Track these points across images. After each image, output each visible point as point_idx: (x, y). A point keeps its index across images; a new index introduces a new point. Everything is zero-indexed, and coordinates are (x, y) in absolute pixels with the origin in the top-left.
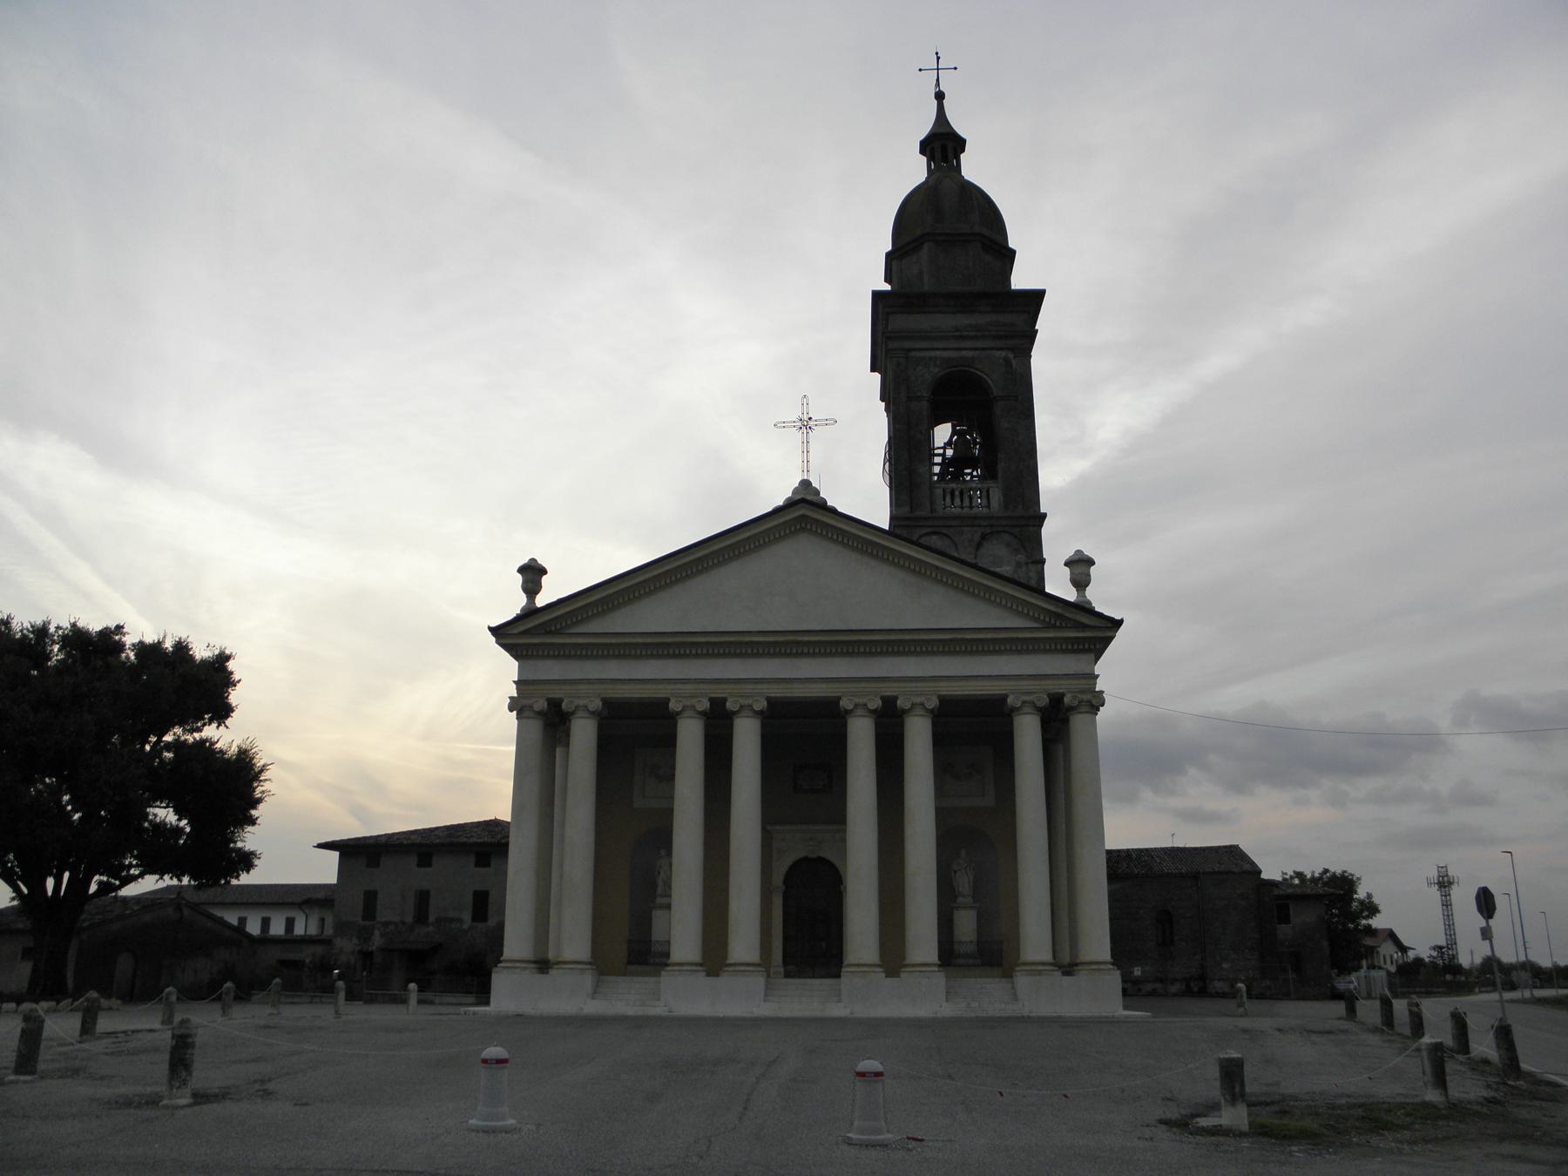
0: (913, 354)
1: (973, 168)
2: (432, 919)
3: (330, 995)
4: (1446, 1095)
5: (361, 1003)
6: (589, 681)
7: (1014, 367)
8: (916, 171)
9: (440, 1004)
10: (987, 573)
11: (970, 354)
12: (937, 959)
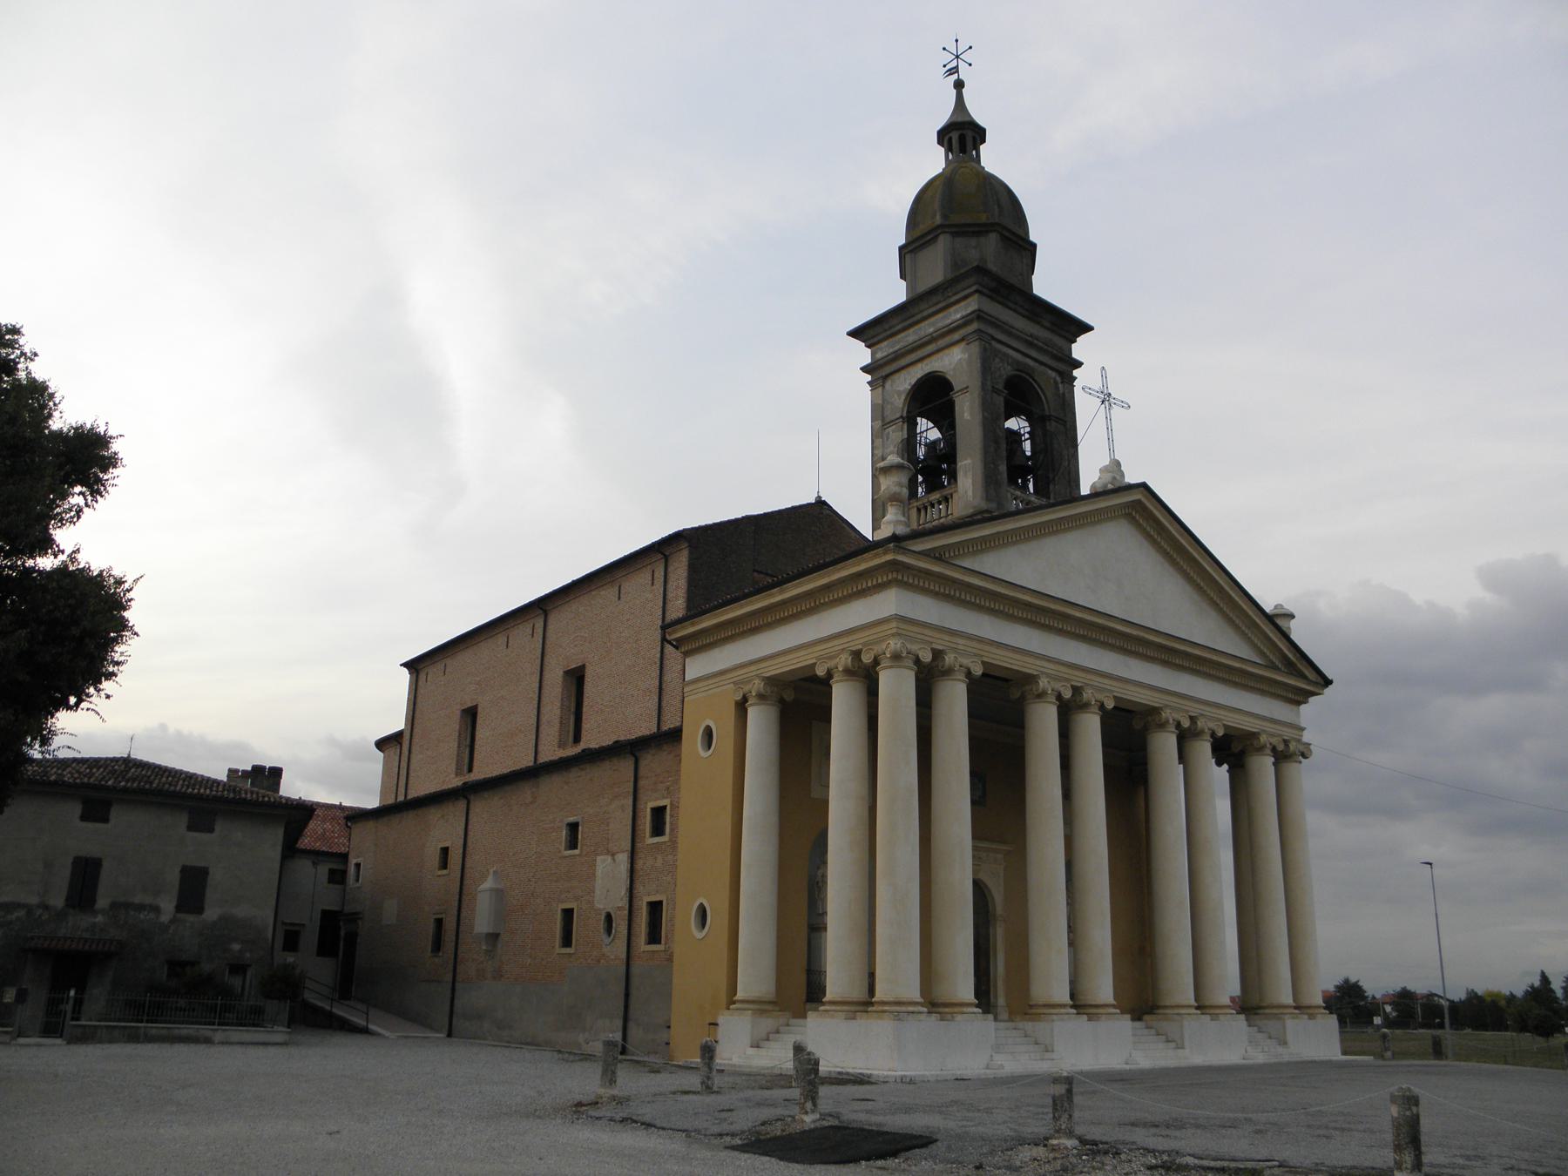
0: (993, 343)
1: (991, 159)
2: (102, 902)
3: (482, 1042)
5: (59, 1041)
6: (970, 637)
7: (1061, 392)
8: (934, 162)
9: (223, 1043)
10: (999, 519)
12: (973, 998)
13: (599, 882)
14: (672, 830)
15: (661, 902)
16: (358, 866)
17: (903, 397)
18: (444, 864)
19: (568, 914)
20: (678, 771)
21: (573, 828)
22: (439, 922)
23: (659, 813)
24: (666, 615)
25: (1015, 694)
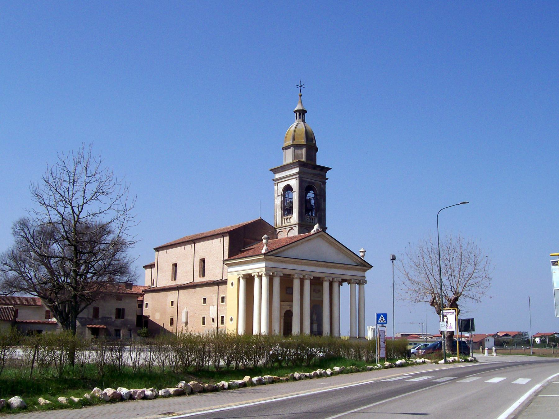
2: (100, 317)
4: (5, 407)
11: (313, 181)
14: (226, 302)
15: (224, 316)
16: (147, 304)
17: (282, 189)
18: (172, 305)
19: (204, 318)
20: (227, 289)
21: (204, 299)
22: (172, 319)
23: (223, 298)
24: (225, 234)
25: (292, 277)
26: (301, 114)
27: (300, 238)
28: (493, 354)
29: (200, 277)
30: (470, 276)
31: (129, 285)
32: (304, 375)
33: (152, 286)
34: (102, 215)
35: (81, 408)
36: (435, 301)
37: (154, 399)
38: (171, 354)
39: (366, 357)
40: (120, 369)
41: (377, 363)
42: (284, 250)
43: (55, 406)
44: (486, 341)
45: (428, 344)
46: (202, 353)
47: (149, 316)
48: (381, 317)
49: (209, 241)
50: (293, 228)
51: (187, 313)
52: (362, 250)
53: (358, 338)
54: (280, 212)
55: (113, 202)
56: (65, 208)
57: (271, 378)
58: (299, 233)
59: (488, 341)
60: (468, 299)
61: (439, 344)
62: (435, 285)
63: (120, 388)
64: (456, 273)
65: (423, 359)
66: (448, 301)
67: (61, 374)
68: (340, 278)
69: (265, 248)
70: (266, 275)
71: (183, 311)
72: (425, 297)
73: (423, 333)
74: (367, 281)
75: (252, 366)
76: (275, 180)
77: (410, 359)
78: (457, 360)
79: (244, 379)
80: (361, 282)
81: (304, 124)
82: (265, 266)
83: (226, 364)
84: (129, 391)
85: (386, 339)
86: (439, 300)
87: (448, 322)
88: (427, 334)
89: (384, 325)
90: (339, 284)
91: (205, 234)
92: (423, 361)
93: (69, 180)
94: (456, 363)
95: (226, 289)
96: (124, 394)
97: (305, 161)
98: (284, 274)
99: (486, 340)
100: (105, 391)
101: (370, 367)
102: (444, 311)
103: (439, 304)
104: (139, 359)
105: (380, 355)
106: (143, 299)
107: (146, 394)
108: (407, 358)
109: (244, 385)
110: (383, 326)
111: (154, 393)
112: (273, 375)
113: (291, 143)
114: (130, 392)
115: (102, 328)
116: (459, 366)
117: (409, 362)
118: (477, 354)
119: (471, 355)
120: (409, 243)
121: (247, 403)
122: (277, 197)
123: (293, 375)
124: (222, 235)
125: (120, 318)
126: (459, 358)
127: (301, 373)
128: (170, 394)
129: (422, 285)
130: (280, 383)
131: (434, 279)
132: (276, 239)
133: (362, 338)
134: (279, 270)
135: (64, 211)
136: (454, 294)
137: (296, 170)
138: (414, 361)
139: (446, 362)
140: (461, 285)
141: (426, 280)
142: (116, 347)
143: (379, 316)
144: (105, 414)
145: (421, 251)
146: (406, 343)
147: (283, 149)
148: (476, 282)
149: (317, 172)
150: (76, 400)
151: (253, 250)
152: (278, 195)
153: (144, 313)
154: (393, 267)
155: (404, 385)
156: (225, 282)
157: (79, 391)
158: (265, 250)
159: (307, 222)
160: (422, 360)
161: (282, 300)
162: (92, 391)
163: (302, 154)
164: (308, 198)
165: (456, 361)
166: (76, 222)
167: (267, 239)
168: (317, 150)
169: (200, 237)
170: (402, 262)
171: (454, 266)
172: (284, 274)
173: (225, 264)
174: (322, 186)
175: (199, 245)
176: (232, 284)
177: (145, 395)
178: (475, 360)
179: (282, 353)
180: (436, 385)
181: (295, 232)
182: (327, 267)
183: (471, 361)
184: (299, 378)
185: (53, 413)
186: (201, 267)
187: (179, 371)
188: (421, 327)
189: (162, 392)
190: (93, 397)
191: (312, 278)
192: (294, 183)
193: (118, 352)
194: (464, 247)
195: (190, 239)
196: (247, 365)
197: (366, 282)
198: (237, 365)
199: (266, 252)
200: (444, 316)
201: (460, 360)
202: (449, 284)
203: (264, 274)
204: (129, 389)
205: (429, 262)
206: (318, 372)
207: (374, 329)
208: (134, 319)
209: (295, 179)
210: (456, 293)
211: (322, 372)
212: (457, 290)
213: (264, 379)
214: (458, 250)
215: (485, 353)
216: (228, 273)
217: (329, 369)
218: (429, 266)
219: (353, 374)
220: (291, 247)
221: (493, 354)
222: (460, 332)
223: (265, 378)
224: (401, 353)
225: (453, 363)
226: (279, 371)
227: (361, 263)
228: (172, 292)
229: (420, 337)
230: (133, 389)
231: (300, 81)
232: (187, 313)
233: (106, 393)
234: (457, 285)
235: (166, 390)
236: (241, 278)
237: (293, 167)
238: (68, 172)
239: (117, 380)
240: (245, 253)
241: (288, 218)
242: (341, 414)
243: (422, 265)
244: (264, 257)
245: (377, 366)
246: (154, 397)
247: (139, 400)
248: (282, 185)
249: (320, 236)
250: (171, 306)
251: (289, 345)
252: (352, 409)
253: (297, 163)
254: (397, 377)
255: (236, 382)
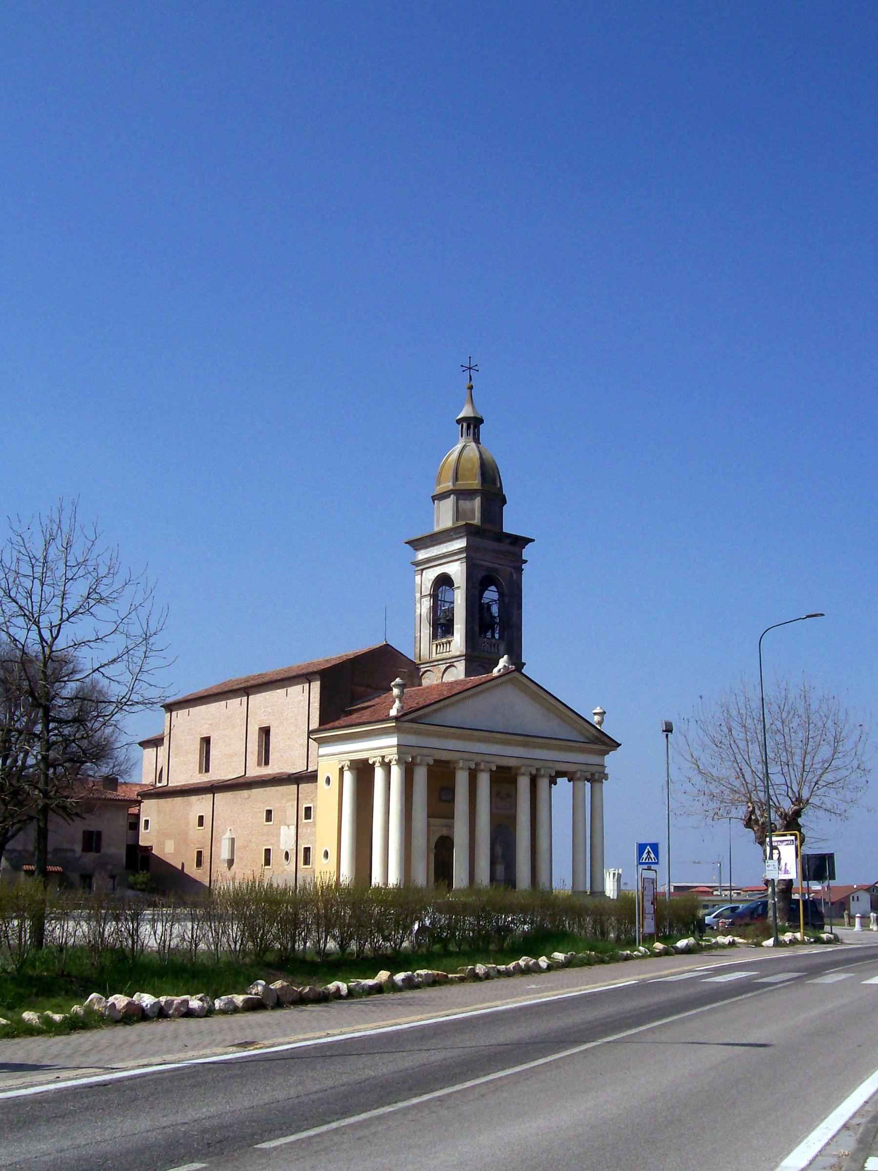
11: (496, 566)
13: (282, 838)
14: (314, 817)
15: (309, 848)
16: (147, 822)
17: (431, 583)
19: (268, 851)
21: (269, 812)
22: (200, 853)
23: (308, 810)
25: (451, 766)
26: (472, 426)
27: (469, 686)
28: (871, 927)
29: (259, 764)
30: (826, 765)
31: (111, 782)
32: (496, 969)
33: (158, 785)
34: (100, 644)
35: (68, 1034)
36: (753, 817)
37: (205, 1016)
38: (232, 926)
39: (614, 933)
40: (134, 957)
41: (639, 945)
42: (436, 711)
43: (18, 1029)
44: (853, 900)
45: (738, 907)
46: (292, 924)
47: (151, 847)
48: (646, 851)
49: (278, 691)
50: (455, 664)
51: (233, 840)
52: (598, 710)
53: (588, 893)
54: (426, 631)
55: (122, 620)
56: (29, 630)
57: (431, 976)
58: (468, 673)
59: (858, 900)
60: (820, 813)
61: (761, 906)
62: (754, 784)
63: (140, 995)
64: (797, 760)
65: (730, 936)
66: (780, 816)
67: (21, 966)
68: (552, 768)
69: (397, 704)
70: (399, 762)
71: (224, 837)
72: (733, 810)
73: (721, 883)
74: (607, 774)
75: (389, 951)
76: (417, 564)
77: (704, 938)
78: (799, 940)
79: (376, 978)
80: (596, 777)
81: (478, 447)
82: (396, 743)
83: (340, 947)
84: (156, 1000)
85: (656, 896)
86: (762, 816)
87: (782, 861)
88: (732, 885)
89: (653, 867)
90: (550, 782)
91: (270, 675)
92: (731, 941)
93: (33, 573)
94: (798, 946)
95: (315, 792)
96: (149, 1006)
97: (480, 524)
98: (435, 761)
99: (853, 897)
100: (111, 999)
101: (625, 953)
102: (774, 839)
103: (763, 823)
104: (171, 935)
105: (645, 929)
106: (139, 812)
107: (191, 1007)
108: (698, 934)
109: (379, 989)
110: (649, 869)
111: (205, 1005)
112: (434, 969)
113: (451, 487)
114: (159, 1002)
115: (55, 872)
116: (806, 952)
117: (703, 943)
118: (837, 927)
119: (827, 928)
120: (701, 697)
121: (395, 1025)
122: (421, 599)
123: (473, 970)
124: (306, 677)
125: (91, 851)
126: (805, 934)
127: (490, 966)
128: (237, 1007)
129: (726, 785)
130: (449, 986)
131: (752, 771)
132: (419, 688)
133: (598, 893)
134: (425, 751)
135: (27, 638)
136: (793, 804)
137: (461, 543)
138: (714, 941)
139: (778, 944)
140: (808, 785)
141: (736, 774)
142: (126, 913)
143: (641, 848)
144: (120, 1046)
145: (725, 715)
146: (696, 903)
147: (435, 498)
148: (838, 778)
149: (504, 547)
150: (57, 1017)
151: (371, 709)
152: (423, 595)
153: (142, 841)
154: (668, 748)
155: (698, 989)
156: (312, 777)
157: (58, 1000)
158: (397, 710)
159: (484, 651)
160: (726, 940)
161: (431, 815)
162: (87, 999)
163: (473, 511)
164: (485, 601)
165: (798, 940)
166: (47, 659)
167: (402, 686)
168: (504, 501)
169: (260, 682)
170: (685, 737)
171: (793, 744)
172: (435, 761)
173: (312, 739)
174: (515, 577)
175: (256, 699)
176: (328, 781)
177: (188, 1008)
178: (836, 940)
179: (448, 924)
180: (766, 990)
181: (458, 672)
182: (526, 745)
183: (829, 942)
184: (485, 975)
185: (17, 1044)
186: (260, 744)
187: (247, 960)
188: (717, 872)
189: (220, 1003)
190: (89, 1011)
191: (494, 768)
192: (457, 570)
193: (130, 923)
194: (814, 707)
195: (238, 687)
196: (379, 947)
197: (606, 777)
198: (360, 948)
199: (400, 714)
200: (773, 848)
201: (806, 940)
202: (784, 782)
203: (395, 760)
204: (157, 998)
205: (742, 735)
206: (522, 962)
207: (619, 875)
208: (121, 852)
209: (459, 562)
210: (799, 800)
211: (531, 963)
212: (799, 794)
213: (417, 977)
214: (801, 711)
215: (854, 926)
216: (319, 758)
217: (544, 958)
218: (742, 744)
219: (592, 967)
220: (453, 704)
221: (871, 927)
222: (806, 882)
223: (418, 974)
224: (686, 925)
225: (792, 946)
226: (446, 962)
227: (596, 736)
228: (201, 797)
229: (715, 893)
230: (165, 997)
231: (470, 358)
232: (233, 840)
233: (113, 1005)
234: (798, 784)
235: (228, 998)
236: (346, 768)
237: (454, 537)
238: (32, 556)
239: (130, 978)
240: (354, 716)
241: (443, 644)
242: (588, 1044)
243: (727, 742)
244: (394, 724)
245: (639, 951)
246: (205, 1013)
247: (177, 1018)
248: (431, 574)
249: (511, 681)
250: (199, 826)
251: (450, 908)
252: (608, 1035)
253: (463, 529)
254: (682, 973)
255: (363, 983)
